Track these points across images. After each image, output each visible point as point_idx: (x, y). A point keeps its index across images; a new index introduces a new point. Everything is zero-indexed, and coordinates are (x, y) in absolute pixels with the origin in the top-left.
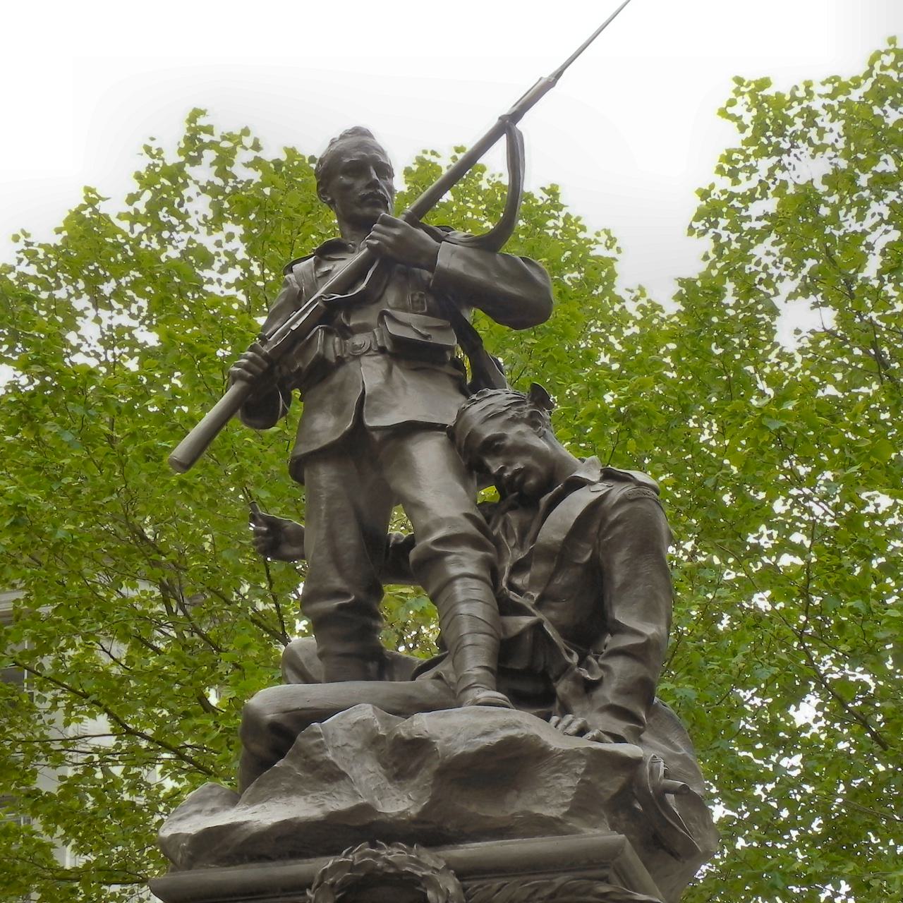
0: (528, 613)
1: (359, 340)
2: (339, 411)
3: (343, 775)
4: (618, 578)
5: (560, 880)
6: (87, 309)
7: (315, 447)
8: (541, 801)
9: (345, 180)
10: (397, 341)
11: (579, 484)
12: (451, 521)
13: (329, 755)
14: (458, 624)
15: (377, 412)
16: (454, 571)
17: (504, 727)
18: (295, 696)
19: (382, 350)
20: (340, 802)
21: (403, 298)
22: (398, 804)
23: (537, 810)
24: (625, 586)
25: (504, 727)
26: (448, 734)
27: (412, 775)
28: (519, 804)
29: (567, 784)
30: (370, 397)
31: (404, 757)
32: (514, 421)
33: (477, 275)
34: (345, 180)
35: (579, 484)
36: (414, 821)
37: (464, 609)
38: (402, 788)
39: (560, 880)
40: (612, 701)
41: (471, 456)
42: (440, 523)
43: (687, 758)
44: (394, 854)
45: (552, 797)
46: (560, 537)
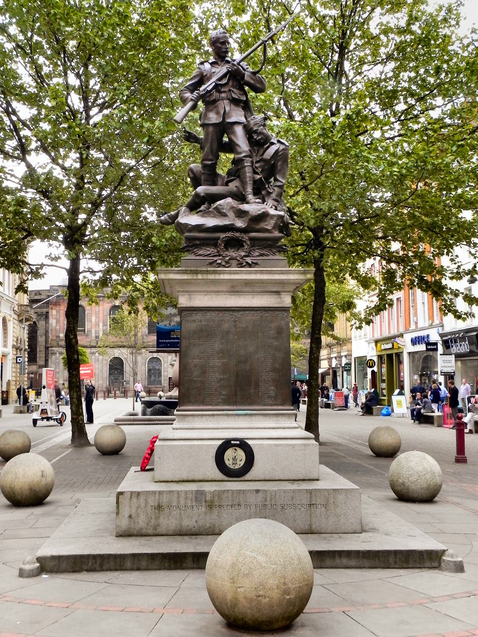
0: (259, 174)
1: (223, 95)
2: (218, 113)
3: (227, 216)
4: (279, 168)
5: (269, 243)
6: (443, 329)
7: (210, 122)
8: (266, 225)
9: (219, 45)
10: (233, 98)
11: (273, 144)
12: (246, 152)
13: (224, 211)
14: (246, 178)
15: (229, 118)
16: (246, 164)
17: (263, 209)
18: (206, 189)
19: (229, 99)
20: (226, 222)
21: (233, 84)
22: (240, 224)
23: (266, 227)
24: (280, 170)
25: (263, 209)
26: (252, 210)
27: (242, 217)
28: (263, 225)
29: (273, 222)
30: (228, 113)
31: (241, 214)
32: (260, 126)
33: (252, 82)
34: (219, 45)
35: (273, 144)
36: (243, 228)
37: (248, 174)
38: (239, 220)
39: (269, 243)
40: (275, 198)
41: (249, 132)
42: (244, 152)
43: (254, 189)
44: (237, 234)
45: (269, 224)
46: (269, 158)
